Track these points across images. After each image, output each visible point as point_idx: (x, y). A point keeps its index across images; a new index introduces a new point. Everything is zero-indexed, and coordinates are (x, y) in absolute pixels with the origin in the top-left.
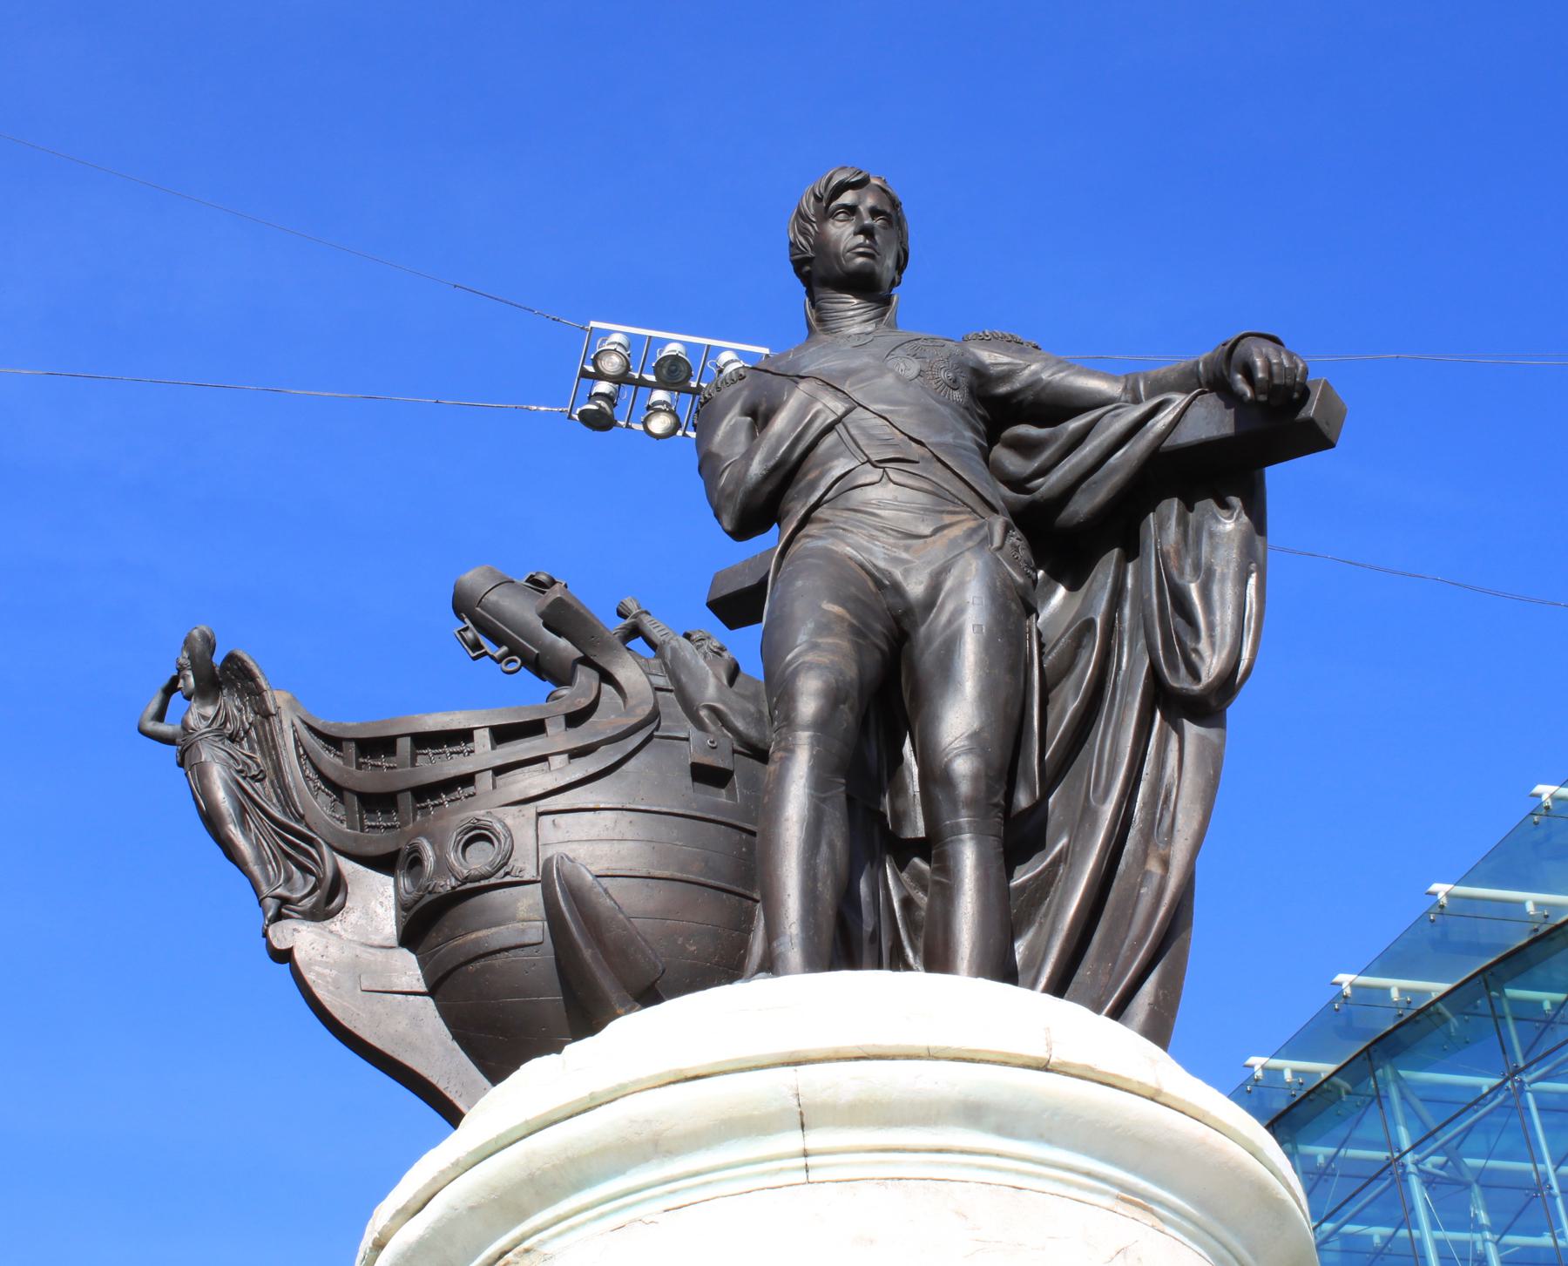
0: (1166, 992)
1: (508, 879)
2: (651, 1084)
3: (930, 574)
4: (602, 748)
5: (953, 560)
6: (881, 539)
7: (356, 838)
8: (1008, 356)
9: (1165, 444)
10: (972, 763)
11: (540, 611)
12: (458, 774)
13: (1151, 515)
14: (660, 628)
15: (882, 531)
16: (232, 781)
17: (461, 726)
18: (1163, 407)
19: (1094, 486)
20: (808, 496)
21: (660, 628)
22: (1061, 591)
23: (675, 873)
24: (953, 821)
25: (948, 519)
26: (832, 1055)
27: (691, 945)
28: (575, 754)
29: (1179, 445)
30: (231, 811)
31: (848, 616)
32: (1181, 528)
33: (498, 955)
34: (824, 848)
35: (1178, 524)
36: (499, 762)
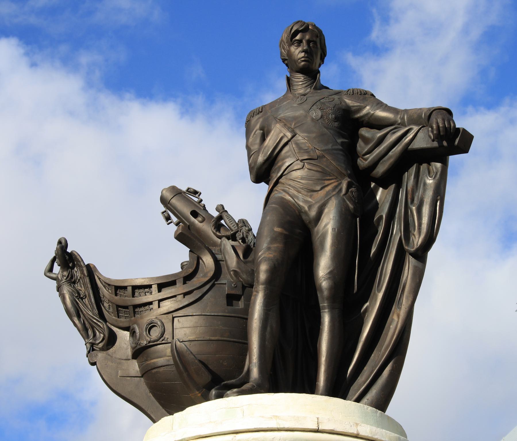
0: (397, 365)
1: (163, 342)
2: (193, 439)
3: (318, 207)
4: (195, 291)
5: (327, 201)
6: (302, 192)
7: (116, 321)
8: (358, 103)
9: (410, 147)
10: (329, 283)
11: (175, 237)
12: (147, 302)
13: (406, 173)
14: (230, 219)
15: (302, 189)
16: (74, 301)
17: (148, 284)
18: (410, 131)
19: (384, 162)
20: (278, 172)
21: (230, 219)
22: (381, 189)
23: (219, 338)
24: (323, 305)
25: (327, 182)
26: (247, 430)
27: (225, 363)
28: (185, 294)
29: (414, 148)
30: (74, 312)
31: (358, 115)
32: (416, 179)
33: (161, 368)
34: (269, 329)
35: (414, 178)
36: (160, 298)
